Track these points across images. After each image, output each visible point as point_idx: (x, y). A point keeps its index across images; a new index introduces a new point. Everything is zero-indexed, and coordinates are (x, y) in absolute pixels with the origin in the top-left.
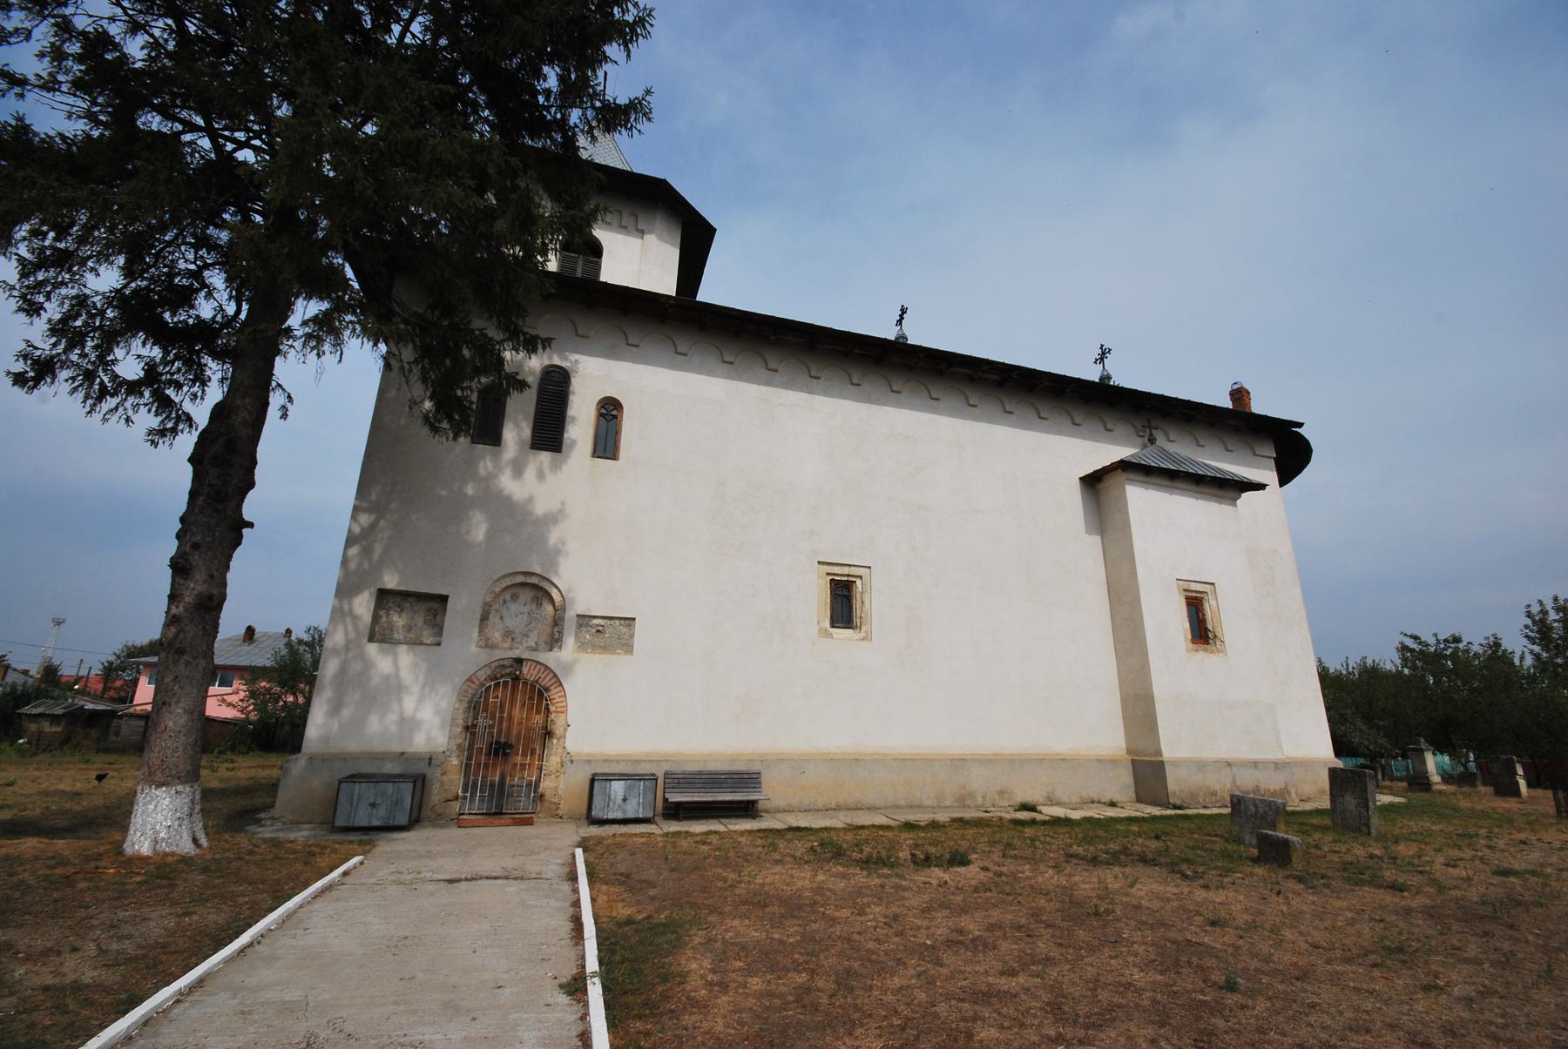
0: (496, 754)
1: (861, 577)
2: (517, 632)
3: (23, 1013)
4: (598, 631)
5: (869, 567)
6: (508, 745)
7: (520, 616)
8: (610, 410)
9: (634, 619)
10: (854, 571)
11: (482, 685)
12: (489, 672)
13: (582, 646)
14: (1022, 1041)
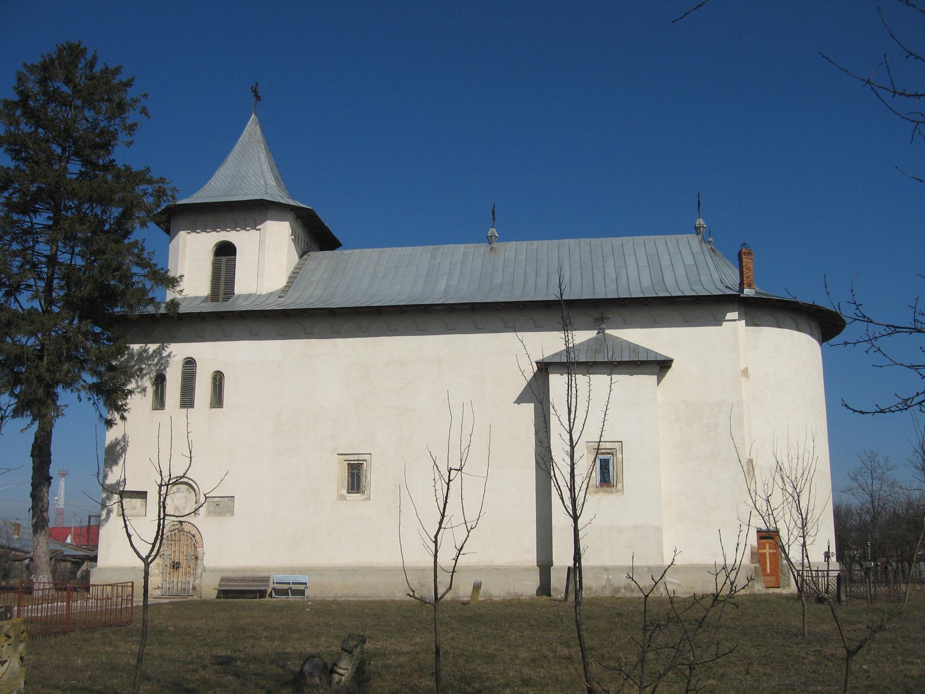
1: (366, 460)
4: (217, 504)
5: (371, 454)
6: (178, 563)
8: (218, 379)
9: (234, 497)
10: (361, 457)
13: (209, 513)
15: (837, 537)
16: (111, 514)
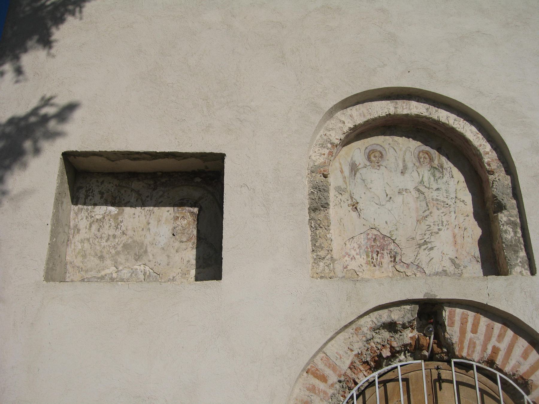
2: (401, 237)
3: (395, 259)
7: (399, 199)
12: (358, 346)
14: (341, 391)
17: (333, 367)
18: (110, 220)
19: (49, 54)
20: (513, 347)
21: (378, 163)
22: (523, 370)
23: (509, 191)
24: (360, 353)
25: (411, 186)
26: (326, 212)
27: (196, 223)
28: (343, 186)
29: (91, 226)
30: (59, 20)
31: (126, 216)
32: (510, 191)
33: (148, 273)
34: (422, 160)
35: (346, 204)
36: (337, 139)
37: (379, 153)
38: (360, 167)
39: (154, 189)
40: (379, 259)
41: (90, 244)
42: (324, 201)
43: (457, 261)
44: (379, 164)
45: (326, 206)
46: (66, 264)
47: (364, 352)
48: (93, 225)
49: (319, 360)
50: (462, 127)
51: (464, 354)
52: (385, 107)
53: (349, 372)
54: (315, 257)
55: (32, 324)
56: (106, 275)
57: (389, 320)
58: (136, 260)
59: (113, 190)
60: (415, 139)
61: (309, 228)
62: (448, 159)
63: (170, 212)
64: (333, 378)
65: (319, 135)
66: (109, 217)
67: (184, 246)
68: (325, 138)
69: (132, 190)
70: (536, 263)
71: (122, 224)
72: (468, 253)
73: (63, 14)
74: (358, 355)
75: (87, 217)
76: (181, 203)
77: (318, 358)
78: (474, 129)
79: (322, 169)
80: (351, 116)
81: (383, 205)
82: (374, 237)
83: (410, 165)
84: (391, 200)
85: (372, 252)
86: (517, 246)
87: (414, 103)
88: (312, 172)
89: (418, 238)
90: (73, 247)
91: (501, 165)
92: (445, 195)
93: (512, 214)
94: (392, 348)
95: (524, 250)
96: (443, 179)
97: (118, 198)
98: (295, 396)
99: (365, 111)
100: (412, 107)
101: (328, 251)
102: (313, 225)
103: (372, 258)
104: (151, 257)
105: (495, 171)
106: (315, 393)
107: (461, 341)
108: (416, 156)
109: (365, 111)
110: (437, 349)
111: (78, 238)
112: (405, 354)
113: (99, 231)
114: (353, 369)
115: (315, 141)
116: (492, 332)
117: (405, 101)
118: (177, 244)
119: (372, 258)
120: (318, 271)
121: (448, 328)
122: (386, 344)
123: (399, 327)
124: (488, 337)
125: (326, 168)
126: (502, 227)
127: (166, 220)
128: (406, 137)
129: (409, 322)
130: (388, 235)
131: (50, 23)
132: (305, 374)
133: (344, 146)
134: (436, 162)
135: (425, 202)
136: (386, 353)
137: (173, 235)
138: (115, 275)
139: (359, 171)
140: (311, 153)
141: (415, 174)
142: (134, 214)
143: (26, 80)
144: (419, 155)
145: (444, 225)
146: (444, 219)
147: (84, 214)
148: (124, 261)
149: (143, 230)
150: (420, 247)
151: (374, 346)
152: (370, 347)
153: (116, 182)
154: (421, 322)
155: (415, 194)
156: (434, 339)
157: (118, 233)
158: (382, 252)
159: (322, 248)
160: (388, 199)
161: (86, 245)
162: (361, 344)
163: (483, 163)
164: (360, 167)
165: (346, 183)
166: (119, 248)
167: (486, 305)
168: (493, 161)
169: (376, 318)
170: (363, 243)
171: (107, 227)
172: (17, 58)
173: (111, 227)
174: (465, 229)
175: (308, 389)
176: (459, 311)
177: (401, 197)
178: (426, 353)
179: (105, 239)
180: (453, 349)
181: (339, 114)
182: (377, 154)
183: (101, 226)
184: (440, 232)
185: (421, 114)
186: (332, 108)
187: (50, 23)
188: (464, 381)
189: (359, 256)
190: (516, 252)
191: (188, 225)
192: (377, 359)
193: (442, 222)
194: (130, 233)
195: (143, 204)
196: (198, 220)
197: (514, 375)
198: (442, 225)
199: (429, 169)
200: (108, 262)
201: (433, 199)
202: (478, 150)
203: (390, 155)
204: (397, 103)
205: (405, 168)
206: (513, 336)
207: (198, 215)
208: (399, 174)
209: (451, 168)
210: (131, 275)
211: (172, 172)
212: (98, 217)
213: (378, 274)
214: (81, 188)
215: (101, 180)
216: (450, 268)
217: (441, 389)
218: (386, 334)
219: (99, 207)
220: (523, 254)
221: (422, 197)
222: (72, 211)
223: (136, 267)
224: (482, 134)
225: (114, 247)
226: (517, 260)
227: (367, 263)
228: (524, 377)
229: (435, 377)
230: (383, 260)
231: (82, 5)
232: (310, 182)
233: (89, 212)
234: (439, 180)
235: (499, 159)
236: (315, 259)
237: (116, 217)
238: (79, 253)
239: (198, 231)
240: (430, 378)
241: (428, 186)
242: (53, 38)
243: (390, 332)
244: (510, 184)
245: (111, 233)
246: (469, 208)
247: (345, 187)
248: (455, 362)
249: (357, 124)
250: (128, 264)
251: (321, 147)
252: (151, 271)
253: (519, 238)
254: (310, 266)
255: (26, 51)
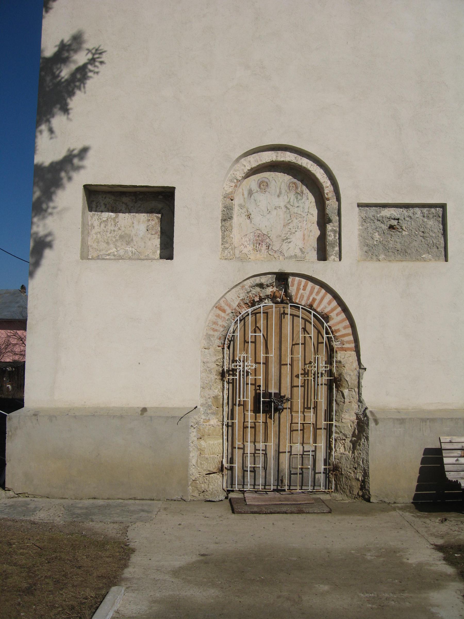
0: (267, 411)
2: (273, 236)
7: (274, 212)
11: (236, 313)
12: (242, 296)
15: (271, 403)
16: (47, 253)
17: (229, 306)
18: (111, 221)
19: (68, 119)
20: (324, 298)
21: (265, 189)
22: (326, 311)
23: (336, 211)
24: (243, 298)
25: (282, 204)
26: (231, 221)
27: (160, 223)
28: (243, 204)
29: (100, 225)
30: (71, 94)
31: (120, 219)
32: (336, 211)
33: (134, 252)
34: (291, 188)
35: (244, 215)
36: (240, 177)
37: (266, 183)
38: (254, 192)
39: (136, 202)
40: (260, 248)
41: (101, 235)
42: (230, 216)
43: (303, 250)
44: (265, 190)
45: (231, 218)
46: (88, 247)
47: (246, 298)
48: (102, 224)
49: (222, 302)
50: (315, 169)
51: (297, 301)
52: (270, 156)
53: (237, 308)
54: (223, 248)
55: (76, 282)
56: (111, 253)
57: (260, 282)
58: (127, 245)
59: (111, 203)
60: (288, 174)
61: (221, 231)
62: (307, 187)
63: (145, 217)
64: (229, 311)
65: (230, 174)
66: (110, 219)
67: (153, 236)
68: (233, 176)
69: (123, 203)
70: (342, 255)
71: (118, 224)
72: (310, 245)
73: (73, 89)
74: (242, 300)
75: (98, 219)
76: (151, 211)
77: (222, 301)
78: (322, 171)
79: (230, 196)
80: (249, 162)
81: (265, 216)
82: (258, 235)
83: (283, 191)
84: (270, 213)
85: (256, 243)
86: (335, 244)
87: (288, 153)
88: (225, 197)
89: (283, 236)
90: (91, 237)
91: (335, 194)
92: (302, 210)
93: (335, 225)
94: (260, 296)
95: (338, 247)
96: (302, 201)
97: (115, 208)
98: (209, 319)
99: (258, 159)
100: (286, 156)
101: (230, 244)
102: (223, 229)
103: (256, 247)
104: (135, 243)
105: (330, 199)
106: (219, 318)
107: (297, 294)
108: (288, 185)
109: (258, 159)
110: (285, 298)
111: (94, 231)
112: (268, 300)
113: (105, 227)
114: (240, 307)
115: (227, 178)
116: (314, 290)
117: (283, 152)
118: (149, 236)
119: (256, 247)
120: (224, 255)
121: (290, 287)
122: (257, 294)
123: (265, 286)
124: (311, 293)
125: (233, 195)
126: (328, 233)
127: (143, 221)
128: (283, 173)
129: (270, 284)
130: (266, 234)
131: (66, 95)
132: (215, 308)
133: (245, 179)
134: (299, 189)
135: (289, 214)
136: (257, 299)
137: (147, 230)
138: (116, 253)
139: (254, 194)
140: (225, 185)
141: (286, 197)
142: (125, 218)
143: (56, 137)
144: (289, 185)
145: (299, 228)
146: (299, 225)
147: (96, 217)
148: (121, 245)
149: (130, 227)
150: (283, 241)
151: (251, 295)
152: (249, 295)
153: (113, 198)
154: (279, 283)
155: (284, 209)
156: (284, 292)
157: (116, 229)
158: (262, 243)
159: (227, 243)
160: (268, 212)
161: (99, 236)
162: (244, 294)
163: (324, 193)
164: (254, 192)
165: (245, 202)
166: (117, 238)
167: (311, 276)
168: (330, 192)
169: (253, 281)
170: (252, 238)
171: (110, 225)
172: (48, 121)
173: (112, 225)
174: (311, 231)
175: (216, 316)
176: (297, 279)
177: (276, 211)
178: (279, 300)
179: (109, 232)
180: (292, 298)
181: (242, 160)
182: (265, 184)
183: (106, 225)
184: (296, 233)
185: (291, 161)
186: (238, 158)
187: (66, 95)
188: (297, 315)
189: (249, 246)
190: (334, 247)
191: (155, 225)
192: (252, 302)
193: (298, 227)
194: (123, 229)
195: (129, 211)
196: (161, 221)
197: (322, 312)
198: (298, 229)
199: (294, 194)
200: (112, 246)
201: (294, 213)
202: (323, 185)
203: (273, 185)
204: (278, 153)
205: (280, 193)
206: (325, 293)
207: (161, 218)
208: (277, 197)
209: (307, 194)
210: (125, 253)
211: (146, 192)
212: (104, 219)
213: (258, 256)
214: (93, 201)
215: (104, 196)
216: (299, 254)
217: (284, 318)
218: (258, 289)
219: (104, 213)
220: (337, 249)
221: (288, 211)
222: (89, 215)
223: (127, 248)
224: (326, 175)
225: (115, 237)
226: (333, 252)
227: (253, 250)
228: (327, 314)
229: (282, 312)
230: (262, 248)
231: (85, 82)
232: (223, 204)
233: (99, 216)
234: (299, 201)
235: (334, 191)
236: (223, 249)
237: (114, 219)
238: (95, 240)
239: (161, 228)
240: (279, 312)
241: (292, 204)
242: (70, 106)
243: (260, 288)
244: (337, 207)
245: (112, 229)
246: (315, 219)
247: (245, 204)
248: (290, 305)
249: (253, 167)
250: (123, 247)
251: (230, 182)
252: (135, 251)
253: (336, 239)
254: (220, 253)
255: (53, 116)
